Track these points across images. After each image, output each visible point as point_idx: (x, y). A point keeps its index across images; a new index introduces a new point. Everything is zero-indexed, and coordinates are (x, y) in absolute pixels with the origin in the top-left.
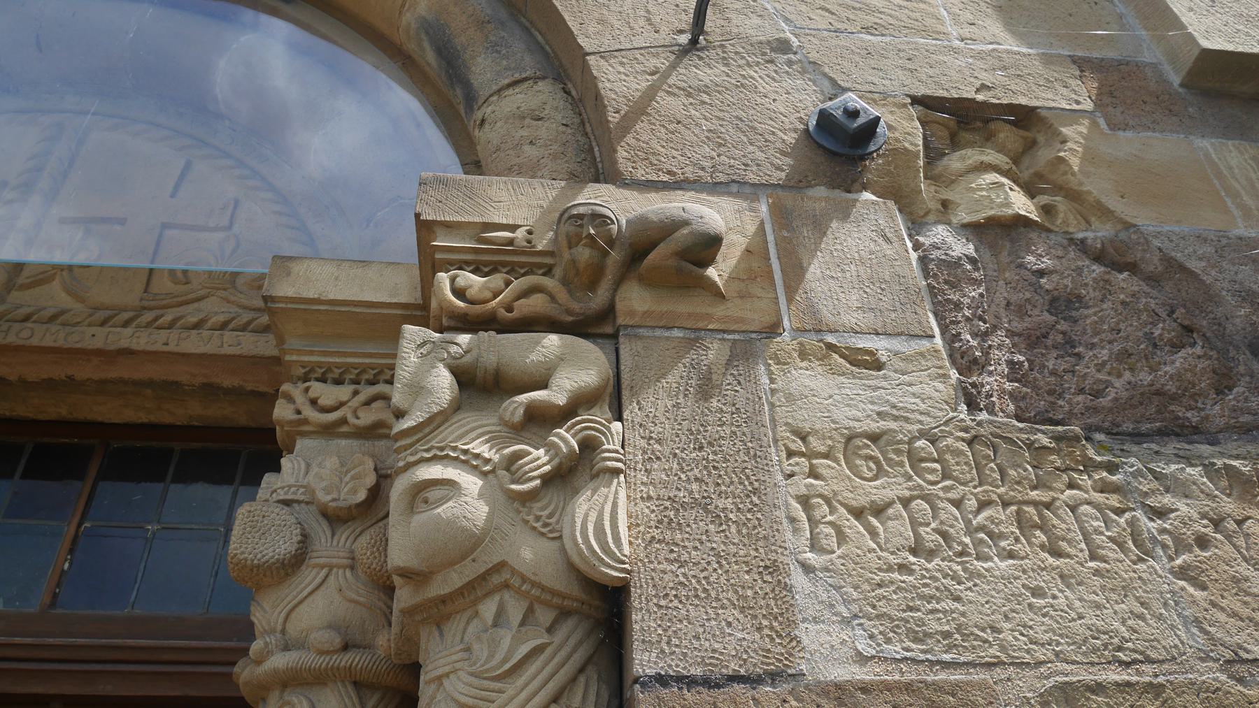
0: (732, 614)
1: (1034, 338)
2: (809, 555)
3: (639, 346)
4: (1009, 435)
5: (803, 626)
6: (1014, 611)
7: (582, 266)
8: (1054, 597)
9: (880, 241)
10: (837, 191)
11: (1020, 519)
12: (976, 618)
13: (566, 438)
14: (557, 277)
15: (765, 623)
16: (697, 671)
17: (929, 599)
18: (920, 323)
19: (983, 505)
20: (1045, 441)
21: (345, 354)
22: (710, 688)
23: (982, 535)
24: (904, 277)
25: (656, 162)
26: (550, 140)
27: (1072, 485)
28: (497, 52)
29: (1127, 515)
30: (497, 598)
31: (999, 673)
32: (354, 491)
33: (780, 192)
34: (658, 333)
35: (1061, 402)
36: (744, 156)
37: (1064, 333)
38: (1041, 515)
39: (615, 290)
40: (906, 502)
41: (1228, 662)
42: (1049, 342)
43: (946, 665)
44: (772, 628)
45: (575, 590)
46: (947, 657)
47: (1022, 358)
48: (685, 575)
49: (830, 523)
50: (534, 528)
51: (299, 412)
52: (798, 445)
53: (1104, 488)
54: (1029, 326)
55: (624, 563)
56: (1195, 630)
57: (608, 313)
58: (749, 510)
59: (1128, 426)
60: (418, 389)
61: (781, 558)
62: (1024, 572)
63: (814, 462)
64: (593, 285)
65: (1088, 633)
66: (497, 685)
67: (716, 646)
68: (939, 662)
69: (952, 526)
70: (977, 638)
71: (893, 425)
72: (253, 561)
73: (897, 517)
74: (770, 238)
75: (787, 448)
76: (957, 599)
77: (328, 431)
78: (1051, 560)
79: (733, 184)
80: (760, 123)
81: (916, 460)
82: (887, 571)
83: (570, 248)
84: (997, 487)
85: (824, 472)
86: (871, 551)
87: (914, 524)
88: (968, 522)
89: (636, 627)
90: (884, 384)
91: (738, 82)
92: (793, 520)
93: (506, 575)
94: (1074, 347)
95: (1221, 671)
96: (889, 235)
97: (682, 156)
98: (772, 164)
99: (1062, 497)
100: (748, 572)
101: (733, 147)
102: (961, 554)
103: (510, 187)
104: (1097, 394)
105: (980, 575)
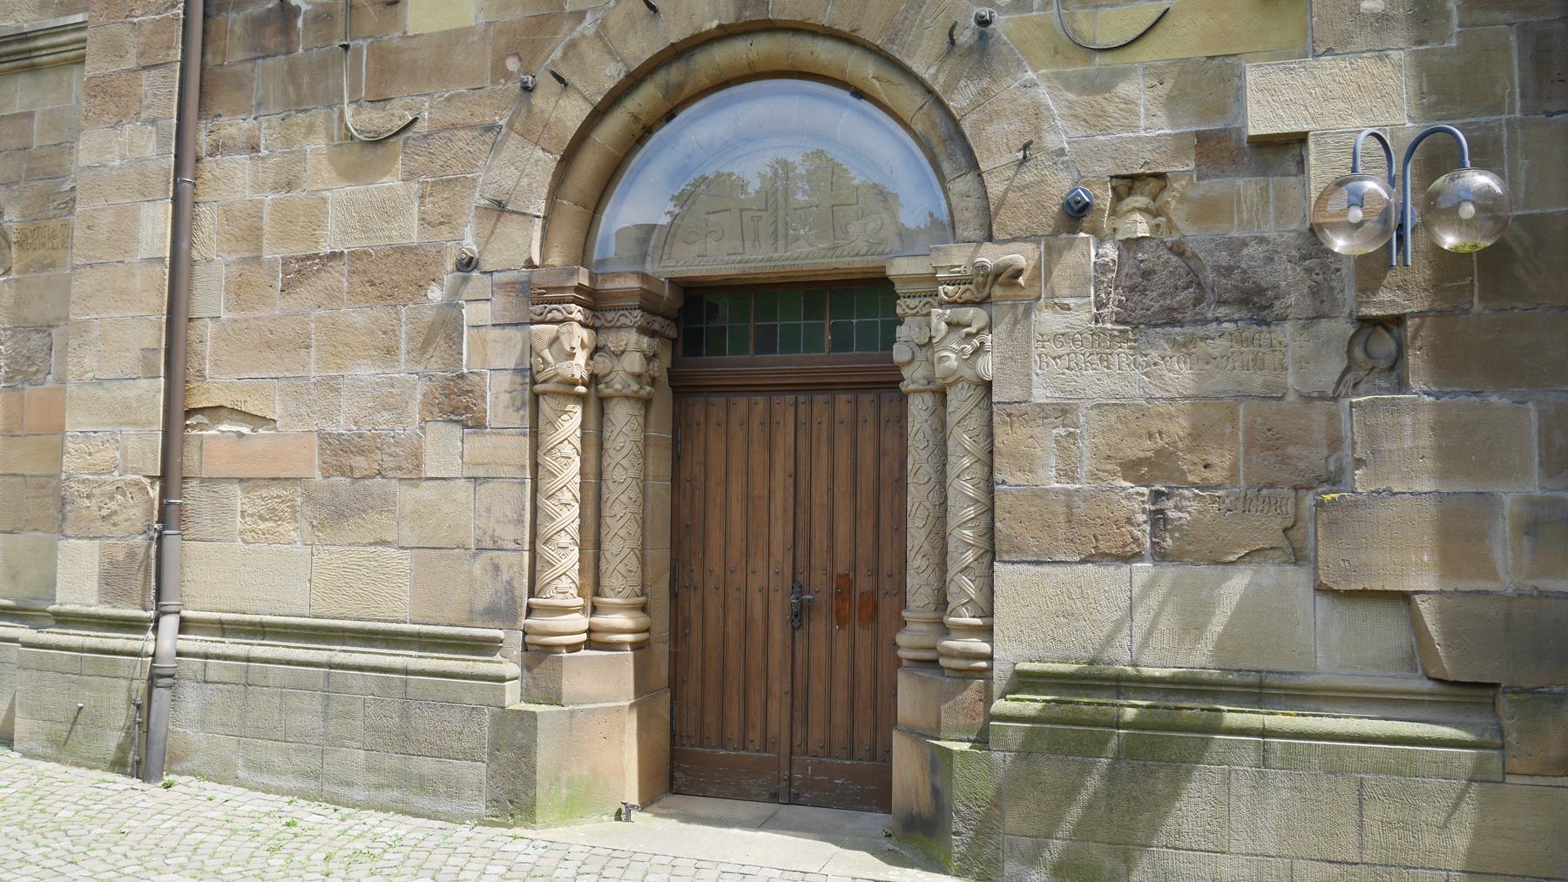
3: (997, 308)
11: (1101, 358)
13: (976, 342)
53: (1130, 348)
60: (937, 330)
64: (984, 286)
77: (914, 315)
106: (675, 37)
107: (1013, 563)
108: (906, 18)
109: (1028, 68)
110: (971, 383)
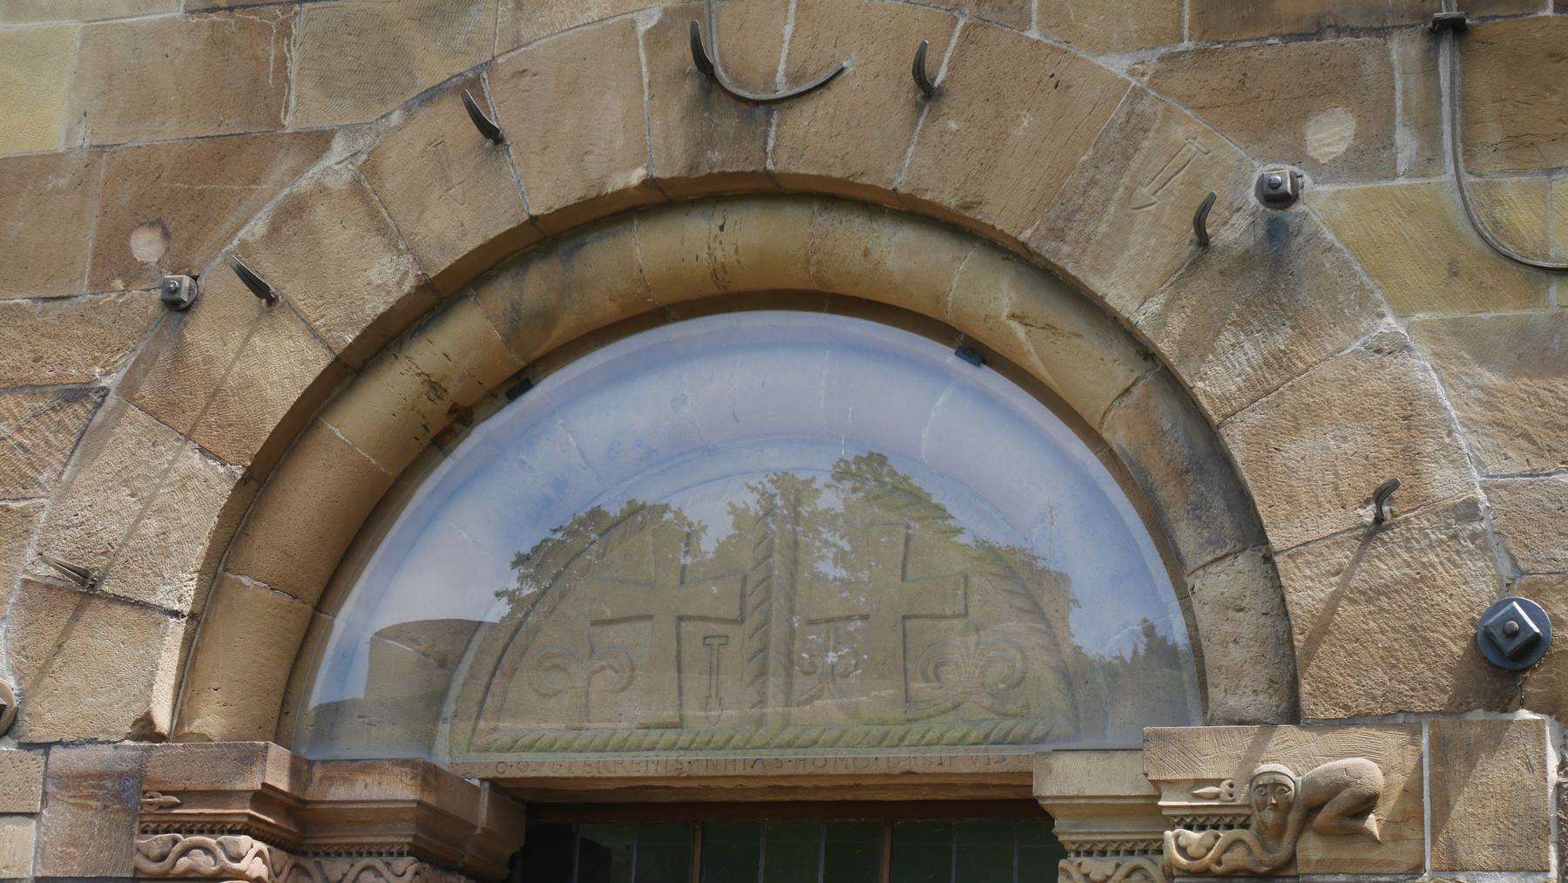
7: (1269, 825)
10: (1494, 713)
18: (1539, 858)
21: (1106, 833)
24: (1536, 809)
25: (1334, 695)
26: (1251, 639)
28: (1199, 518)
33: (1441, 719)
36: (1413, 678)
39: (1296, 842)
74: (1426, 774)
80: (1433, 632)
91: (1418, 573)
97: (1358, 684)
98: (1438, 686)
101: (1406, 667)
103: (1214, 738)
106: (541, 201)
108: (1093, 182)
109: (1384, 308)
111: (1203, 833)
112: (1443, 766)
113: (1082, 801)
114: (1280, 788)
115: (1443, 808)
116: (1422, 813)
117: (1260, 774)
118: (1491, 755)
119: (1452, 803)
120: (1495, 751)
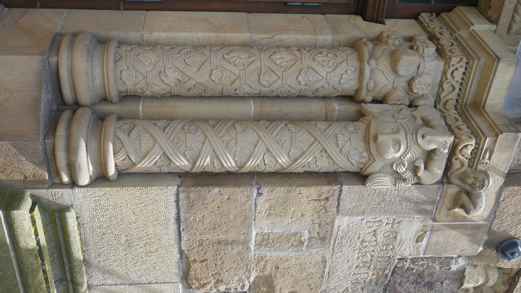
0: (354, 204)
1: (420, 275)
2: (366, 220)
4: (389, 265)
5: (349, 217)
6: (344, 256)
8: (346, 264)
9: (462, 249)
10: (485, 242)
11: (366, 262)
12: (344, 249)
14: (467, 169)
15: (351, 211)
16: (342, 197)
17: (351, 241)
18: (429, 253)
19: (372, 256)
20: (386, 272)
21: (473, 79)
22: (338, 199)
23: (364, 254)
27: (373, 274)
29: (363, 283)
30: (367, 156)
31: (331, 251)
32: (418, 89)
34: (439, 194)
35: (399, 276)
37: (421, 283)
38: (367, 266)
40: (376, 241)
41: (326, 291)
42: (419, 278)
43: (335, 242)
44: (349, 212)
45: (367, 172)
46: (336, 242)
47: (414, 272)
48: (365, 196)
49: (373, 225)
50: (383, 167)
51: (453, 65)
52: (396, 221)
54: (425, 275)
55: (370, 187)
56: (334, 287)
57: (449, 183)
58: (380, 210)
59: (388, 288)
61: (366, 215)
62: (353, 260)
63: (391, 224)
65: (337, 268)
66: (346, 156)
67: (347, 201)
68: (336, 240)
69: (367, 249)
70: (340, 248)
71: (398, 242)
72: (399, 64)
73: (372, 238)
74: (469, 223)
75: (396, 219)
76: (349, 246)
77: (444, 73)
78: (355, 266)
79: (494, 216)
81: (387, 245)
82: (359, 234)
83: (474, 177)
84: (376, 260)
85: (387, 226)
86: (364, 232)
87: (370, 242)
88: (368, 252)
89: (354, 186)
90: (411, 242)
92: (375, 218)
93: (372, 160)
94: (416, 283)
95: (324, 289)
96: (463, 252)
98: (500, 227)
99: (370, 272)
100: (364, 208)
102: (360, 249)
104: (400, 285)
105: (354, 252)
107: (177, 201)
110: (366, 165)
111: (470, 154)
112: (471, 228)
113: (491, 77)
114: (481, 187)
115: (455, 228)
116: (456, 221)
117: (489, 181)
118: (469, 241)
119: (456, 230)
120: (471, 242)
